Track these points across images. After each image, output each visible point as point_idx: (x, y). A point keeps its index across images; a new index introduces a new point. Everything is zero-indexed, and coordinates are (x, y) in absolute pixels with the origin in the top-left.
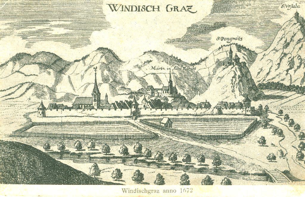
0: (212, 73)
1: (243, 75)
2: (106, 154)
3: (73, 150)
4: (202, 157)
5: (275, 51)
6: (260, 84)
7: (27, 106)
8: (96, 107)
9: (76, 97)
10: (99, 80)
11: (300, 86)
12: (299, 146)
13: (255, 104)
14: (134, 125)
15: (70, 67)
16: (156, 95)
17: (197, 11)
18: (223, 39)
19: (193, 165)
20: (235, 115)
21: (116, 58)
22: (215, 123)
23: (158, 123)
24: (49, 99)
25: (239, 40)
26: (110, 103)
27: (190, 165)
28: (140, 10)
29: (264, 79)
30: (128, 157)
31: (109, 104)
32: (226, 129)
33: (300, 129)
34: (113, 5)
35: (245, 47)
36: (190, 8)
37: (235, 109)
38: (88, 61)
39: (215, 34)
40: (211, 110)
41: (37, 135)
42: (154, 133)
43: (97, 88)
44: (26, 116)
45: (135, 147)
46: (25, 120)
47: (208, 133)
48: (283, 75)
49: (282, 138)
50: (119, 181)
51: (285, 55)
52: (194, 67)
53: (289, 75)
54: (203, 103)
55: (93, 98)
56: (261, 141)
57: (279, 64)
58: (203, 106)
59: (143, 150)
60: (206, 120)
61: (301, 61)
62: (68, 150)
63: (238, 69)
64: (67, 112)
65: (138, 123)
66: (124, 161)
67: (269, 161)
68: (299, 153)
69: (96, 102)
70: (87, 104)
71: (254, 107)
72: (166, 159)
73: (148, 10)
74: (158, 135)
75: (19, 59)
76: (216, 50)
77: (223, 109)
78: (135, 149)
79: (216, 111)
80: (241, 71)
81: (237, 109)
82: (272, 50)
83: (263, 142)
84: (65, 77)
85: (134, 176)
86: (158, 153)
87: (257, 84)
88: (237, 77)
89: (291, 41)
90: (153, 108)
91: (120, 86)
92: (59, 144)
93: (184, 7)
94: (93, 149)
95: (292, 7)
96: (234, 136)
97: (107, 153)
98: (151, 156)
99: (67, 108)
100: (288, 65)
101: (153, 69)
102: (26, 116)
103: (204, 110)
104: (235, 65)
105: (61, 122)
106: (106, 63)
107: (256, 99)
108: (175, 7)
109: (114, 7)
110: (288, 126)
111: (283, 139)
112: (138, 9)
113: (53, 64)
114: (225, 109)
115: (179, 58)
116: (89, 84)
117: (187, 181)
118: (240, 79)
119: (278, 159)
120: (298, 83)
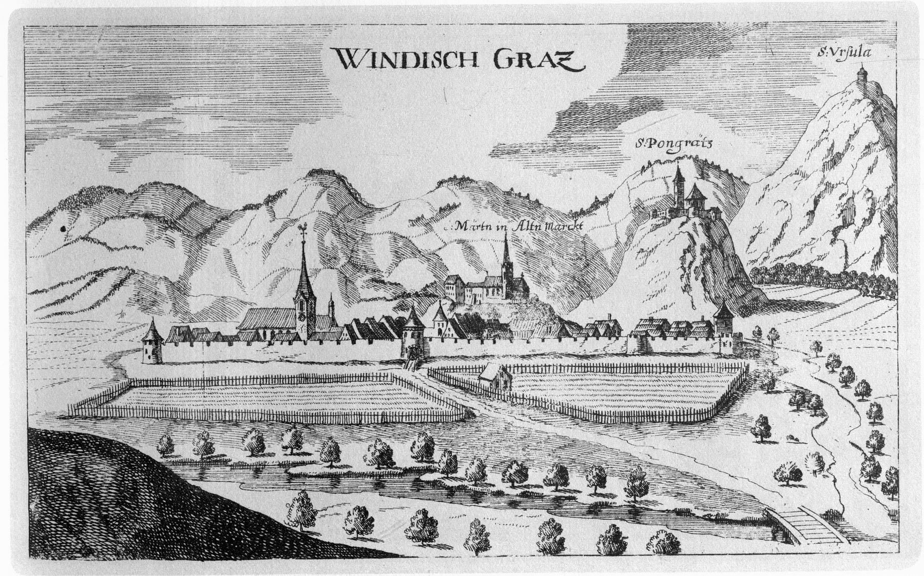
0: (623, 239)
1: (713, 242)
2: (331, 466)
3: (239, 455)
4: (598, 471)
5: (798, 177)
6: (756, 269)
7: (114, 333)
8: (304, 336)
9: (248, 307)
10: (313, 262)
11: (870, 274)
12: (868, 443)
13: (741, 325)
14: (410, 385)
15: (230, 225)
16: (469, 301)
17: (585, 66)
18: (652, 142)
19: (574, 495)
20: (690, 355)
21: (356, 199)
22: (631, 378)
23: (474, 379)
24: (172, 313)
25: (703, 146)
26: (341, 324)
27: (567, 495)
28: (429, 64)
29: (765, 255)
30: (394, 475)
31: (337, 326)
32: (662, 396)
33: (869, 395)
34: (348, 50)
35: (718, 167)
36: (564, 56)
37: (691, 340)
38: (280, 207)
39: (632, 128)
40: (622, 341)
41: (149, 413)
42: (463, 406)
43: (308, 282)
44: (113, 361)
45: (416, 446)
46: (110, 373)
47: (614, 406)
48: (823, 246)
49: (823, 420)
50: (363, 539)
51: (830, 187)
52: (578, 222)
53: (839, 245)
54: (600, 322)
55: (298, 311)
56: (757, 429)
57: (811, 213)
58: (602, 331)
59: (437, 455)
60: (610, 369)
61: (873, 204)
62: (224, 455)
63: (700, 229)
64: (220, 349)
65: (423, 379)
66: (379, 485)
67: (781, 483)
68: (868, 463)
69: (305, 323)
70: (279, 328)
71: (741, 334)
72: (494, 478)
73: (449, 63)
74: (474, 411)
75: (89, 203)
76: (634, 176)
77: (653, 339)
78: (416, 450)
79: (633, 344)
80: (707, 229)
81: (697, 339)
82: (791, 175)
83: (764, 431)
84: (213, 252)
85: (412, 524)
86: (473, 463)
87: (748, 270)
88: (698, 249)
89: (846, 149)
90: (462, 337)
91: (368, 276)
92: (197, 440)
93: (547, 55)
94: (298, 451)
95: (849, 54)
96: (687, 415)
97: (334, 464)
98: (455, 471)
99: (218, 337)
100: (839, 215)
101: (461, 228)
102: (113, 361)
103: (604, 341)
104: (691, 215)
105: (200, 377)
106: (332, 213)
107: (746, 311)
108: (520, 55)
109: (351, 57)
110: (839, 385)
111: (823, 423)
112: (422, 61)
113: (182, 216)
114: (659, 340)
115: (532, 198)
116: (288, 270)
117: (558, 539)
118: (705, 255)
119: (807, 478)
120: (863, 267)
